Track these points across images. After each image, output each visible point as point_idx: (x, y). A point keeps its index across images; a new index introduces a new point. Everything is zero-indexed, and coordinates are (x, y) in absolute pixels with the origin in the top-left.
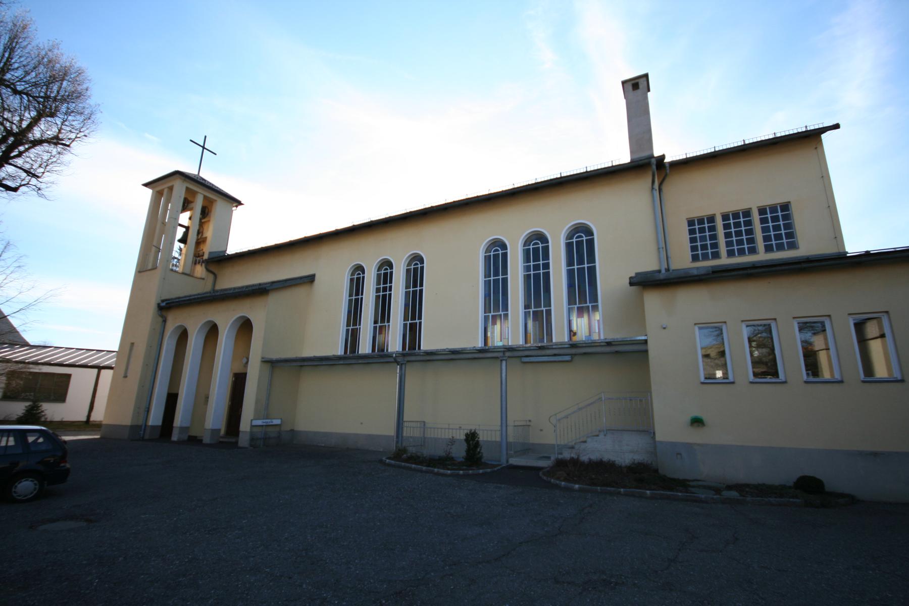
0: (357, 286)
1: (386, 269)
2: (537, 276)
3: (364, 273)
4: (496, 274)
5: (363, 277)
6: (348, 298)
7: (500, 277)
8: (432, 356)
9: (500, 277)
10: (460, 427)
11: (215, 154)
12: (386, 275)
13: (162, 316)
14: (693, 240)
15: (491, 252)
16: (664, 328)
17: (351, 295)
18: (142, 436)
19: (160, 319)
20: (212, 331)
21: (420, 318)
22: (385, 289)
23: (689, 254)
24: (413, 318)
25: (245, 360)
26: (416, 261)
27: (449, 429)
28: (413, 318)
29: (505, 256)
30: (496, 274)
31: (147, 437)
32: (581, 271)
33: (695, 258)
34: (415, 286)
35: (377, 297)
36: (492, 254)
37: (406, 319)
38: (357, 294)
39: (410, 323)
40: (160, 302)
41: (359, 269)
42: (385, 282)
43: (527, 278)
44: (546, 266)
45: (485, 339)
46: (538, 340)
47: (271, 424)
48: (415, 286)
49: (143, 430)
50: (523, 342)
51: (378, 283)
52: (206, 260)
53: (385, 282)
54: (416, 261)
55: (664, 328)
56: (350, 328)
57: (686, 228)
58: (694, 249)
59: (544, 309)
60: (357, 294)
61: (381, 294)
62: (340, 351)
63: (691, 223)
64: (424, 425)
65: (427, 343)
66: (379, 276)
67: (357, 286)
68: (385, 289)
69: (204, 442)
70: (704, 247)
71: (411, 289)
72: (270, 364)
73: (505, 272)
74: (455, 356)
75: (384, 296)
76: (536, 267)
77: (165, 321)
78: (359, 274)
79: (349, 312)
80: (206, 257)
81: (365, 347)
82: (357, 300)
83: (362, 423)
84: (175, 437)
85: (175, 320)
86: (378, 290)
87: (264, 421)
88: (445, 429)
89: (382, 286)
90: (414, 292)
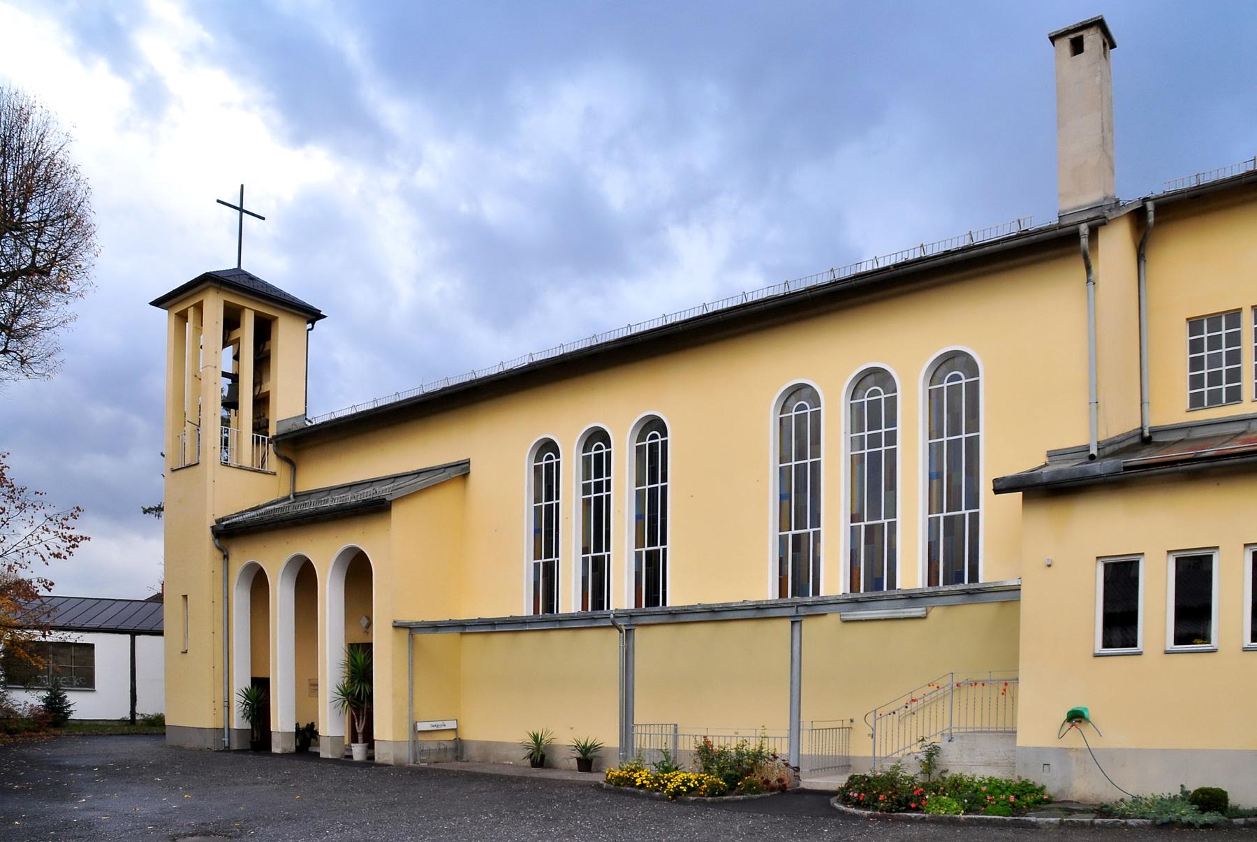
0: (547, 481)
1: (654, 437)
2: (874, 458)
3: (664, 434)
4: (955, 429)
5: (665, 444)
6: (635, 489)
7: (964, 436)
8: (680, 616)
9: (964, 436)
10: (736, 733)
11: (242, 186)
12: (598, 458)
13: (220, 549)
14: (1196, 364)
15: (864, 398)
16: (1049, 566)
17: (537, 500)
18: (227, 744)
19: (219, 555)
20: (305, 577)
21: (664, 542)
22: (598, 487)
23: (1185, 392)
24: (652, 542)
25: (364, 622)
26: (653, 426)
27: (843, 728)
28: (652, 542)
29: (973, 389)
30: (955, 429)
31: (235, 746)
32: (954, 446)
33: (1196, 402)
34: (653, 480)
35: (586, 502)
36: (945, 385)
37: (639, 543)
38: (549, 498)
39: (945, 518)
40: (214, 524)
41: (548, 447)
42: (598, 474)
43: (856, 461)
44: (891, 438)
45: (780, 580)
46: (954, 580)
47: (443, 728)
48: (653, 480)
49: (226, 736)
50: (923, 584)
51: (586, 476)
52: (274, 437)
53: (598, 474)
54: (653, 426)
55: (1049, 566)
56: (541, 561)
57: (1184, 338)
58: (1196, 382)
59: (967, 513)
60: (549, 498)
61: (593, 496)
62: (525, 609)
63: (1195, 325)
64: (676, 730)
65: (676, 595)
66: (586, 460)
67: (547, 481)
68: (598, 487)
69: (321, 756)
70: (1215, 379)
71: (647, 487)
72: (407, 631)
73: (973, 425)
74: (715, 614)
75: (598, 501)
76: (874, 441)
77: (226, 557)
78: (654, 437)
79: (537, 531)
80: (273, 431)
81: (570, 599)
82: (549, 508)
83: (572, 728)
84: (276, 749)
85: (242, 557)
86: (586, 489)
87: (434, 723)
88: (839, 728)
89: (593, 481)
90: (801, 470)
